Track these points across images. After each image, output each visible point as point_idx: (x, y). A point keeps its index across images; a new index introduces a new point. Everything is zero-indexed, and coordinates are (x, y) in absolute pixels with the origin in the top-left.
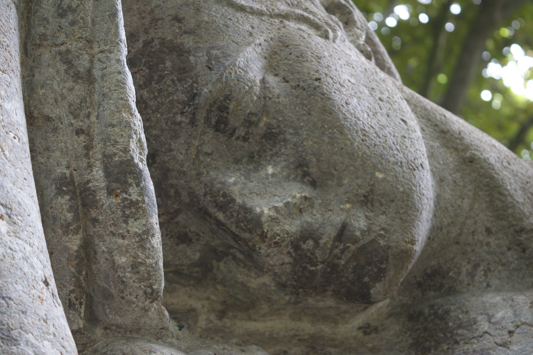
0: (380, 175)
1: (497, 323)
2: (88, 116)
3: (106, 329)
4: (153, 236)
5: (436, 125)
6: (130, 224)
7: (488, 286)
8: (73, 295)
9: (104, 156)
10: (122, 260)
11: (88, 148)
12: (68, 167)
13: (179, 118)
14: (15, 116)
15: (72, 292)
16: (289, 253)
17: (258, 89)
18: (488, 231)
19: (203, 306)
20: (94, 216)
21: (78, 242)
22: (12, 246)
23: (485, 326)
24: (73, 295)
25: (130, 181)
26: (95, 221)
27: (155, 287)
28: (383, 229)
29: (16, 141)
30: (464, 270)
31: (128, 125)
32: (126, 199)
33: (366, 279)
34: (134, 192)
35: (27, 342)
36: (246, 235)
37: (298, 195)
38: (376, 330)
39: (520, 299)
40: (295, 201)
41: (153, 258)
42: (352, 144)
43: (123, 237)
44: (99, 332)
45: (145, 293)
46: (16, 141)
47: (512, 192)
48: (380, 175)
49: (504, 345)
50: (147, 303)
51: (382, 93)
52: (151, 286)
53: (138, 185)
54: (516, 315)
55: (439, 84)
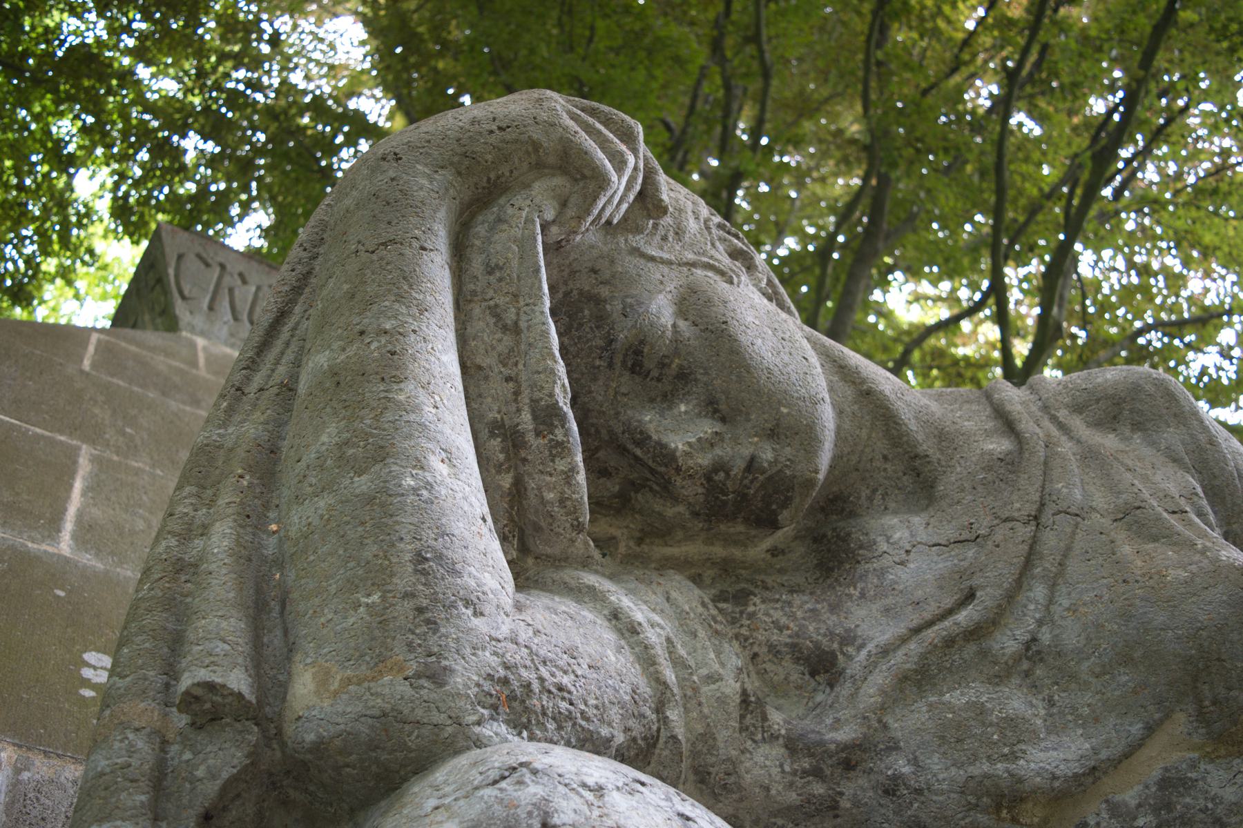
0: (785, 410)
2: (516, 364)
3: (536, 558)
7: (886, 508)
9: (532, 400)
10: (550, 496)
11: (517, 393)
12: (499, 412)
13: (597, 363)
15: (505, 526)
18: (885, 458)
25: (556, 423)
26: (524, 460)
31: (553, 372)
33: (774, 507)
36: (663, 469)
38: (783, 552)
43: (551, 475)
45: (572, 525)
48: (785, 410)
49: (902, 563)
52: (577, 519)
54: (912, 536)
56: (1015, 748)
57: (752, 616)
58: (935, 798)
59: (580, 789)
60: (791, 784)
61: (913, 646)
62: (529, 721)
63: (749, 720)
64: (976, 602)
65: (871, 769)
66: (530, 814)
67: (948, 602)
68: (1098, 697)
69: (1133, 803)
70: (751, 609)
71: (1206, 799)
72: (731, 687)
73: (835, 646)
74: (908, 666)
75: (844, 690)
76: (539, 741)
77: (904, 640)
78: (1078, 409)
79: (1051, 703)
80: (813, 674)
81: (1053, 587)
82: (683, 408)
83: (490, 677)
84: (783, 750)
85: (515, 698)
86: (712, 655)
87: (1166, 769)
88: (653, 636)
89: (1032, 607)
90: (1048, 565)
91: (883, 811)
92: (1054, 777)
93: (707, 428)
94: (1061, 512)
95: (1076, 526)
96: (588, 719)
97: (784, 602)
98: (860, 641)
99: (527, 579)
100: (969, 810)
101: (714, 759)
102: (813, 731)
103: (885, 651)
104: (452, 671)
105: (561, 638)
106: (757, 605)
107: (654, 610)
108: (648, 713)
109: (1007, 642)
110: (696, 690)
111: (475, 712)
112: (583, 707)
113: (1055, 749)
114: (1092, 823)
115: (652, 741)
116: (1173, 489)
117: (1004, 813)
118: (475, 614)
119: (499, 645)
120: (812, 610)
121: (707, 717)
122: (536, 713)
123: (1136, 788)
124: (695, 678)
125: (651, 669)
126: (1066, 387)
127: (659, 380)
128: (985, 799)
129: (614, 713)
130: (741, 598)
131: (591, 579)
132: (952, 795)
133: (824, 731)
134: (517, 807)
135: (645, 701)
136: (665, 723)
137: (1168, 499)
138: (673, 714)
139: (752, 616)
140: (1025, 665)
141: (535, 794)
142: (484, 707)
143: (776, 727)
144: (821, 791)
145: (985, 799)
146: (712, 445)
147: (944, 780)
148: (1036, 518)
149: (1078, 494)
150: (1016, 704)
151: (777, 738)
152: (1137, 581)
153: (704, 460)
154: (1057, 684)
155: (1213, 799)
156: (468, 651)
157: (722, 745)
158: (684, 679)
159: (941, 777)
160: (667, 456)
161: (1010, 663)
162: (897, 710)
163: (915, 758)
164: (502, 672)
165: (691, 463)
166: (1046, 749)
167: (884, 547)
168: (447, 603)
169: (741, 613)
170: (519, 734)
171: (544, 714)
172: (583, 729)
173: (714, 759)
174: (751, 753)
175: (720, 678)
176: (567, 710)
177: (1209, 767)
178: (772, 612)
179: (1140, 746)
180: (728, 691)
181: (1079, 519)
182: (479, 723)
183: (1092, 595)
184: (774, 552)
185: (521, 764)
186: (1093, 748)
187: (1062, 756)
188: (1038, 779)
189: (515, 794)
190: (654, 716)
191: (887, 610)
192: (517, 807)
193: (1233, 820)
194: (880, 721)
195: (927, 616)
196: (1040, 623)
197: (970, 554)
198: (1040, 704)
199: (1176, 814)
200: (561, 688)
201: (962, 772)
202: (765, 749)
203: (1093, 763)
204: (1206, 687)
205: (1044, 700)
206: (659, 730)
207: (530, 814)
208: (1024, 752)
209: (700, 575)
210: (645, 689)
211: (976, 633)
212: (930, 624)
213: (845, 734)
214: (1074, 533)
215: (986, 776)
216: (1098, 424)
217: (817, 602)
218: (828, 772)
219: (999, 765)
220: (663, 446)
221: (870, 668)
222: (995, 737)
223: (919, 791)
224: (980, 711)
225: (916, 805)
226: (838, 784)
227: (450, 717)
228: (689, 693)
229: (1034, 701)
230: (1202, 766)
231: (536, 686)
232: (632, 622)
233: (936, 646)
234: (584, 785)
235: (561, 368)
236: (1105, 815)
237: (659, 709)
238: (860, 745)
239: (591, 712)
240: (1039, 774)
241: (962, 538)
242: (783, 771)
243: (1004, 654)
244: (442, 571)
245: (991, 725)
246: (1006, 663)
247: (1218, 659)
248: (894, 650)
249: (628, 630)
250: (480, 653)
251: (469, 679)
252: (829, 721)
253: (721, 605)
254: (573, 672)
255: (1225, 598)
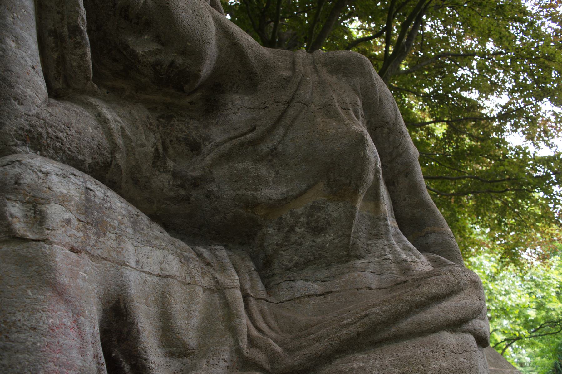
0: (189, 44)
1: (235, 105)
2: (62, 7)
3: (73, 89)
4: (87, 56)
5: (224, 29)
6: (77, 50)
7: (237, 92)
8: (56, 75)
9: (68, 23)
10: (74, 64)
11: (62, 19)
12: (53, 26)
13: (110, 13)
14: (26, 3)
15: (55, 74)
16: (151, 70)
17: (142, 4)
18: (239, 71)
19: (128, 87)
20: (64, 46)
21: (57, 55)
22: (16, 52)
23: (230, 106)
24: (56, 75)
25: (77, 34)
26: (65, 48)
27: (88, 75)
28: (189, 65)
29: (25, 13)
30: (229, 85)
31: (78, 12)
32: (76, 41)
33: (182, 83)
34: (79, 39)
35: (18, 88)
36: (133, 61)
37: (155, 48)
38: (194, 104)
39: (246, 98)
40: (153, 50)
41: (87, 64)
42: (178, 30)
43: (75, 55)
44: (71, 90)
45: (84, 77)
46: (25, 13)
47: (250, 58)
48: (189, 44)
49: (235, 113)
50: (85, 81)
51: (199, 13)
52: (86, 75)
53: (80, 36)
54: (242, 103)
55: (392, 45)
56: (257, 187)
57: (172, 125)
58: (223, 201)
59: (39, 173)
60: (172, 189)
61: (228, 145)
62: (41, 148)
63: (158, 163)
64: (255, 131)
65: (204, 187)
66: (12, 178)
67: (246, 130)
68: (294, 173)
69: (300, 213)
70: (172, 123)
71: (326, 215)
72: (150, 149)
73: (201, 141)
74: (224, 152)
75: (200, 158)
76: (45, 156)
77: (225, 142)
78: (325, 65)
79: (277, 173)
80: (192, 150)
81: (287, 130)
82: (146, 37)
83: (21, 129)
84: (171, 176)
85: (34, 138)
86: (144, 137)
87: (314, 202)
88: (113, 125)
89: (277, 136)
90: (287, 121)
91: (206, 203)
92: (270, 199)
93: (154, 46)
94: (298, 102)
95: (303, 108)
96: (72, 151)
97: (186, 122)
98: (211, 140)
99: (69, 97)
100: (236, 207)
101: (140, 176)
102: (184, 171)
103: (218, 145)
104: (4, 124)
105: (65, 119)
106: (175, 122)
107: (119, 116)
108: (106, 153)
109: (264, 148)
110: (133, 148)
111: (13, 141)
112: (69, 146)
113: (274, 189)
114: (284, 218)
115: (107, 166)
116: (348, 100)
117: (249, 210)
118: (19, 104)
119: (29, 117)
120: (196, 126)
121: (137, 159)
122: (44, 145)
123: (302, 208)
124: (133, 144)
125: (111, 138)
126: (325, 55)
127: (138, 24)
128: (242, 204)
129: (87, 152)
130: (170, 118)
131: (92, 100)
132: (230, 200)
133: (188, 172)
134: (7, 175)
135: (105, 149)
136: (115, 159)
137: (344, 104)
138: (118, 156)
139: (172, 125)
140: (270, 157)
141: (17, 171)
142: (19, 140)
143: (169, 167)
144: (183, 193)
145: (242, 204)
146: (156, 54)
147: (228, 195)
148: (288, 103)
149: (308, 96)
150: (262, 171)
151: (169, 171)
152: (318, 132)
153: (151, 59)
154: (281, 166)
155: (328, 215)
156: (13, 117)
157: (144, 171)
158: (128, 144)
159: (227, 193)
160: (135, 55)
161: (264, 156)
162: (217, 167)
163: (219, 186)
164: (28, 127)
165: (145, 60)
166: (271, 189)
167: (230, 106)
168: (6, 98)
169: (168, 124)
170: (36, 153)
171: (48, 146)
172: (69, 155)
173: (140, 176)
174: (157, 176)
175: (145, 146)
176: (59, 146)
177: (330, 204)
178: (180, 125)
179: (305, 192)
180: (148, 151)
181: (305, 106)
182: (15, 145)
183: (301, 135)
184: (191, 103)
185: (17, 161)
186: (287, 191)
187: (275, 192)
188: (264, 199)
189: (9, 170)
190: (109, 156)
191: (224, 130)
192: (7, 175)
193: (334, 223)
194: (209, 170)
195: (236, 134)
196: (279, 143)
197: (261, 113)
198: (273, 173)
199: (314, 219)
200: (57, 137)
201: (234, 193)
202: (164, 175)
203: (286, 196)
204: (332, 174)
205: (275, 171)
206: (111, 161)
207: (12, 178)
208: (261, 189)
209: (156, 107)
210: (105, 143)
211: (254, 143)
212: (237, 137)
213: (195, 174)
214: (301, 111)
215: (243, 195)
216: (331, 72)
217: (199, 124)
218: (187, 186)
219: (249, 192)
220: (134, 51)
221: (210, 151)
222: (251, 182)
223: (218, 198)
224: (247, 171)
225: (216, 202)
226: (191, 192)
227: (2, 142)
228: (130, 149)
229: (271, 171)
230: (328, 203)
231: (45, 135)
232: (105, 119)
233: (236, 146)
234: (41, 171)
235: (83, 11)
236: (289, 216)
237: (112, 153)
238: (200, 178)
239: (73, 149)
240: (264, 197)
241: (260, 107)
242: (169, 184)
243: (262, 152)
244: (4, 85)
245: (250, 177)
246: (262, 156)
247: (338, 165)
248: (221, 145)
249: (102, 120)
250: (19, 119)
251: (12, 128)
252: (191, 168)
253: (160, 120)
254: (66, 132)
255: (347, 143)
